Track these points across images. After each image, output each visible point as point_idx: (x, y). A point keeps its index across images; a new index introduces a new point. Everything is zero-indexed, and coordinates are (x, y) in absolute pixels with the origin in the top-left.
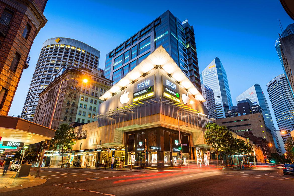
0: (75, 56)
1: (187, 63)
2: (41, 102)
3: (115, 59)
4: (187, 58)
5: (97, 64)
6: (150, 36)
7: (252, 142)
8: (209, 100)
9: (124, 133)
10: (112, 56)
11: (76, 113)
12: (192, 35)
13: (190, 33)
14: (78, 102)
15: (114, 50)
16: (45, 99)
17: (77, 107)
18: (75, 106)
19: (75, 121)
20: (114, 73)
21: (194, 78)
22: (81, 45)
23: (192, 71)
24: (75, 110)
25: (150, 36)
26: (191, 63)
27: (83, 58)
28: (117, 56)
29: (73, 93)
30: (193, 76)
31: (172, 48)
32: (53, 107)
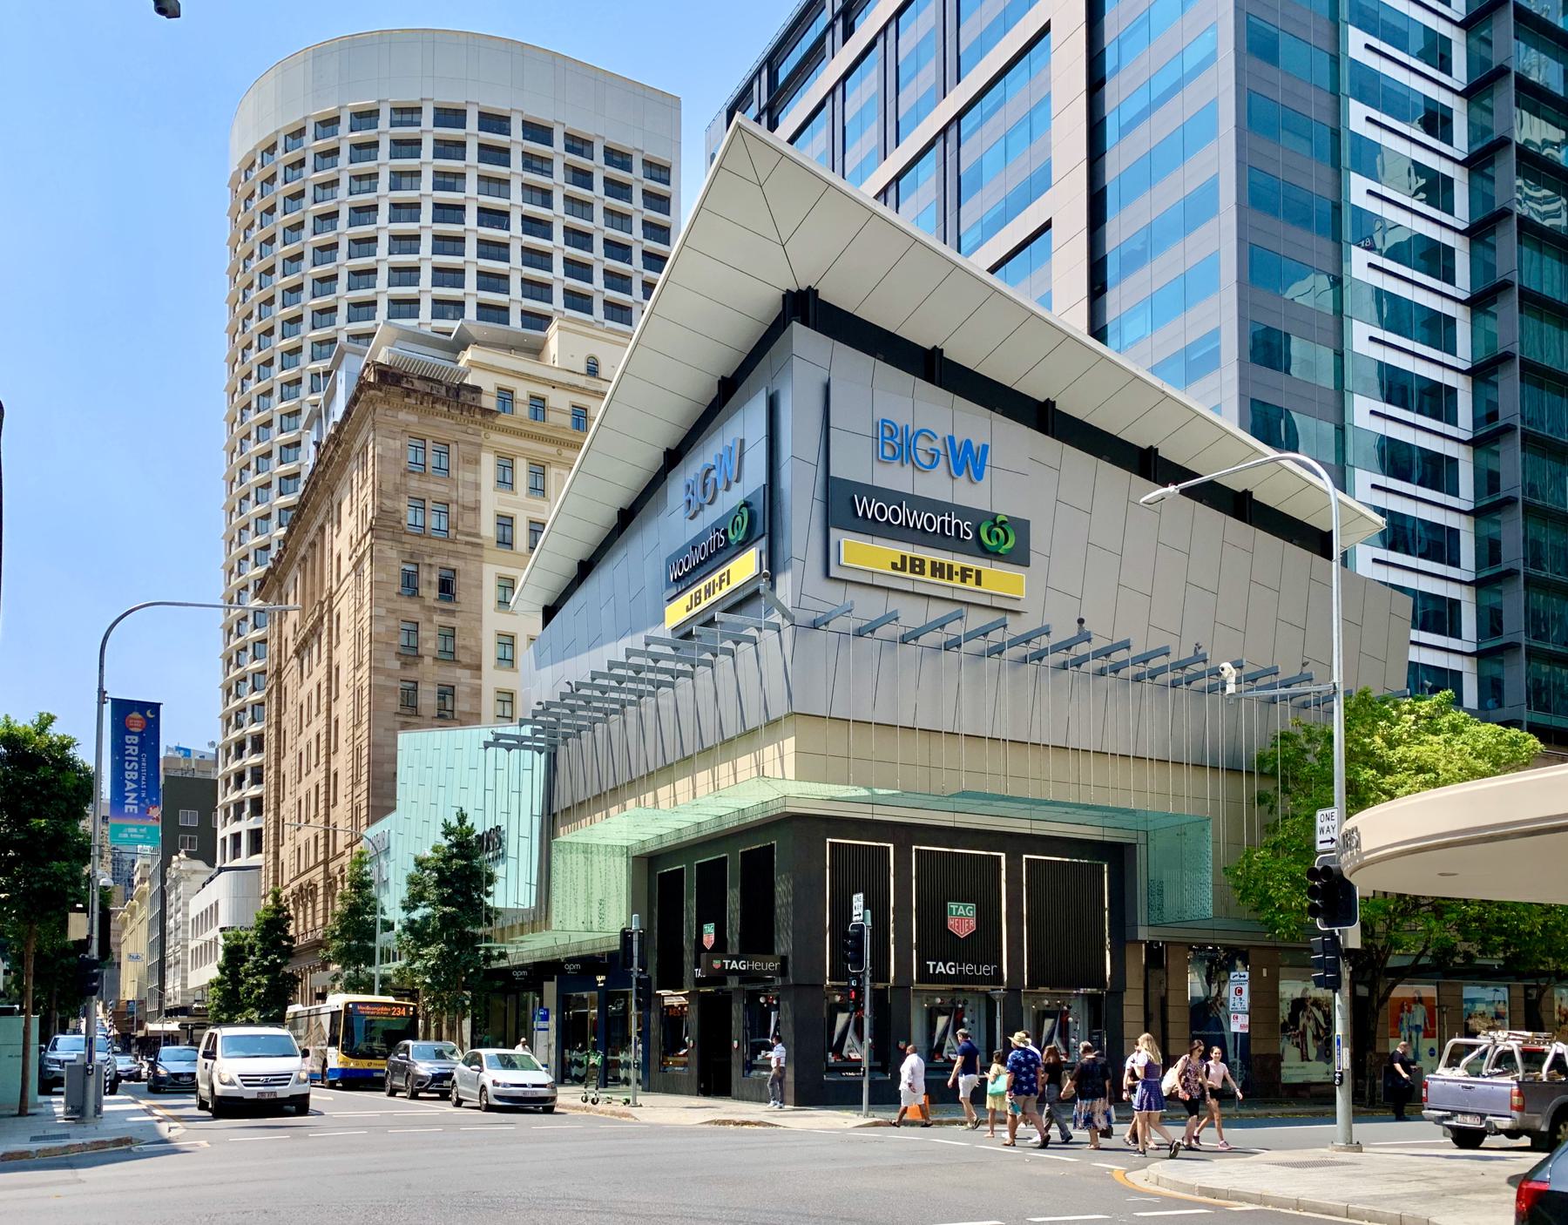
0: (475, 194)
2: (280, 644)
7: (1404, 238)
14: (481, 629)
15: (759, 72)
16: (293, 621)
18: (463, 657)
24: (468, 690)
27: (545, 197)
29: (427, 560)
31: (1481, 1146)
32: (332, 673)
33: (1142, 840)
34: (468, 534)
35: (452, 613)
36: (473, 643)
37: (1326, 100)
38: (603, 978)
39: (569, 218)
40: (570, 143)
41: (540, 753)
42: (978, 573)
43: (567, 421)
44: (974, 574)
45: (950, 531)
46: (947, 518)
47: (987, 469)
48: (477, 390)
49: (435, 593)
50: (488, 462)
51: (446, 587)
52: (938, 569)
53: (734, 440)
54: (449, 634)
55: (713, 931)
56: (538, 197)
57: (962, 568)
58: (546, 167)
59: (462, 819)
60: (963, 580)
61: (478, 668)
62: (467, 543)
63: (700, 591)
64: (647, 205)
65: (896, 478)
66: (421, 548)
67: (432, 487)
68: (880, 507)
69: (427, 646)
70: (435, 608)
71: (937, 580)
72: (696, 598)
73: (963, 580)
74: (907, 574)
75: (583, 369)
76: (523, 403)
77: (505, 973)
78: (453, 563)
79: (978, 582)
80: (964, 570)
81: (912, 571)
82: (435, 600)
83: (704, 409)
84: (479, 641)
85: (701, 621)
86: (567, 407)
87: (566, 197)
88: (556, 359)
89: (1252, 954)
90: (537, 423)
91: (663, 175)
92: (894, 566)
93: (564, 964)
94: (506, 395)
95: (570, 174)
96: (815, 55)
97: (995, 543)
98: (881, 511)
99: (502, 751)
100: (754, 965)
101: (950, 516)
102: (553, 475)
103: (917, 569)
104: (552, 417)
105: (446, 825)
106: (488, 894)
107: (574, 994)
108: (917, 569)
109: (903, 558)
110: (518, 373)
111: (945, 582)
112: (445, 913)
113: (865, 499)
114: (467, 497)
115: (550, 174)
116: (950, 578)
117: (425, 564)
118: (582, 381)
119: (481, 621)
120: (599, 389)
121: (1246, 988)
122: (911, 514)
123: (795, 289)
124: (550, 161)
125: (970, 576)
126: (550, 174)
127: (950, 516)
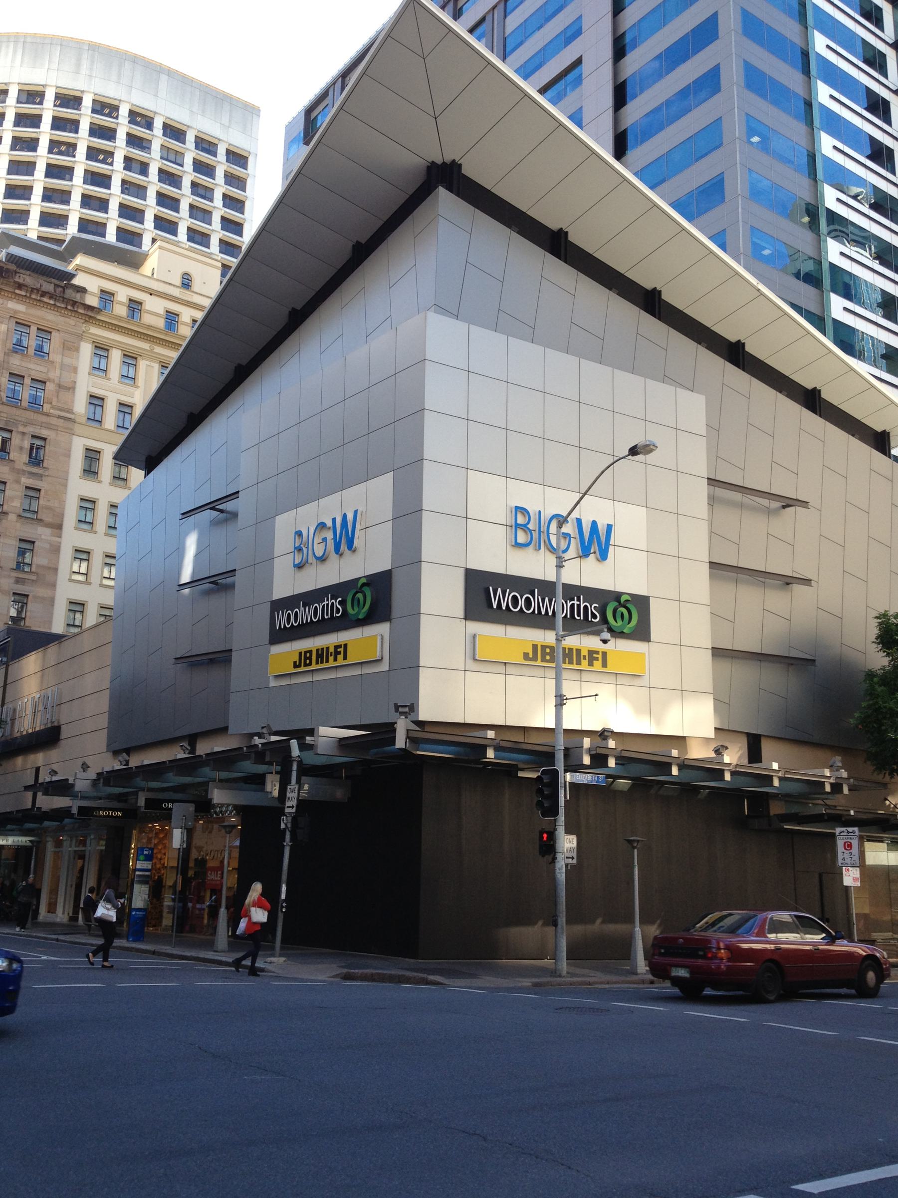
6: (578, 62)
11: (56, 570)
17: (58, 527)
19: (50, 628)
22: (119, 75)
24: (47, 546)
25: (578, 62)
29: (21, 429)
34: (61, 410)
35: (40, 477)
36: (56, 505)
42: (604, 654)
43: (161, 323)
44: (600, 656)
45: (579, 615)
46: (576, 602)
47: (611, 548)
48: (82, 290)
49: (25, 458)
50: (86, 349)
51: (36, 457)
54: (33, 492)
57: (589, 651)
60: (591, 664)
61: (59, 527)
62: (60, 417)
66: (17, 418)
67: (31, 366)
68: (514, 597)
69: (14, 504)
70: (24, 471)
72: (306, 658)
73: (591, 664)
74: (539, 663)
75: (178, 281)
78: (44, 433)
79: (604, 665)
80: (591, 652)
81: (543, 660)
82: (25, 463)
84: (62, 503)
86: (162, 312)
92: (526, 656)
94: (107, 296)
97: (620, 623)
98: (515, 600)
101: (579, 600)
103: (548, 657)
104: (147, 319)
108: (548, 650)
109: (535, 647)
111: (574, 666)
113: (499, 590)
114: (66, 379)
116: (579, 663)
117: (18, 432)
118: (176, 292)
119: (65, 486)
125: (597, 659)
127: (579, 600)
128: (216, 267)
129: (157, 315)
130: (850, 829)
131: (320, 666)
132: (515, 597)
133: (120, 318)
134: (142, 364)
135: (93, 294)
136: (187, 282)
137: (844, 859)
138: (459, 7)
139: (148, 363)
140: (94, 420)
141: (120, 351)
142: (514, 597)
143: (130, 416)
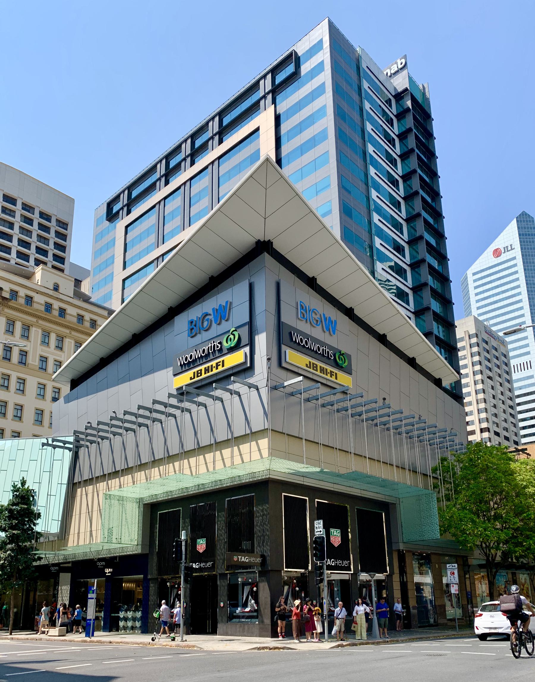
1: (400, 212)
3: (127, 227)
4: (403, 239)
5: (63, 248)
6: (258, 129)
8: (489, 378)
9: (141, 506)
10: (118, 212)
12: (425, 120)
13: (414, 115)
20: (129, 228)
21: (429, 317)
23: (426, 315)
25: (258, 129)
26: (418, 235)
28: (136, 212)
30: (426, 284)
33: (398, 502)
37: (367, 235)
38: (110, 570)
39: (21, 235)
40: (24, 207)
41: (70, 451)
44: (334, 374)
45: (326, 354)
46: (324, 348)
52: (322, 370)
53: (227, 302)
55: (339, 535)
56: (8, 225)
58: (12, 214)
59: (23, 483)
63: (201, 370)
64: (56, 236)
65: (303, 327)
71: (322, 375)
73: (331, 376)
74: (311, 370)
76: (22, 297)
77: (46, 567)
80: (331, 372)
83: (197, 289)
85: (195, 386)
86: (43, 302)
87: (20, 227)
88: (39, 281)
89: (433, 558)
90: (29, 307)
91: (65, 226)
92: (307, 365)
93: (96, 562)
94: (14, 294)
95: (23, 218)
96: (152, 188)
97: (341, 362)
99: (50, 448)
100: (252, 560)
101: (325, 347)
102: (33, 331)
105: (14, 486)
106: (35, 525)
107: (82, 580)
108: (315, 369)
110: (21, 284)
111: (324, 376)
112: (14, 534)
115: (14, 217)
118: (51, 293)
120: (58, 297)
121: (456, 572)
122: (312, 344)
123: (262, 240)
124: (14, 212)
126: (14, 217)
127: (325, 347)
128: (71, 281)
129: (41, 304)
130: (453, 565)
131: (208, 375)
132: (301, 339)
133: (21, 305)
134: (33, 330)
135: (7, 292)
136: (56, 288)
137: (451, 580)
138: (273, 105)
139: (35, 329)
140: (6, 358)
141: (20, 323)
142: (301, 338)
143: (25, 357)
